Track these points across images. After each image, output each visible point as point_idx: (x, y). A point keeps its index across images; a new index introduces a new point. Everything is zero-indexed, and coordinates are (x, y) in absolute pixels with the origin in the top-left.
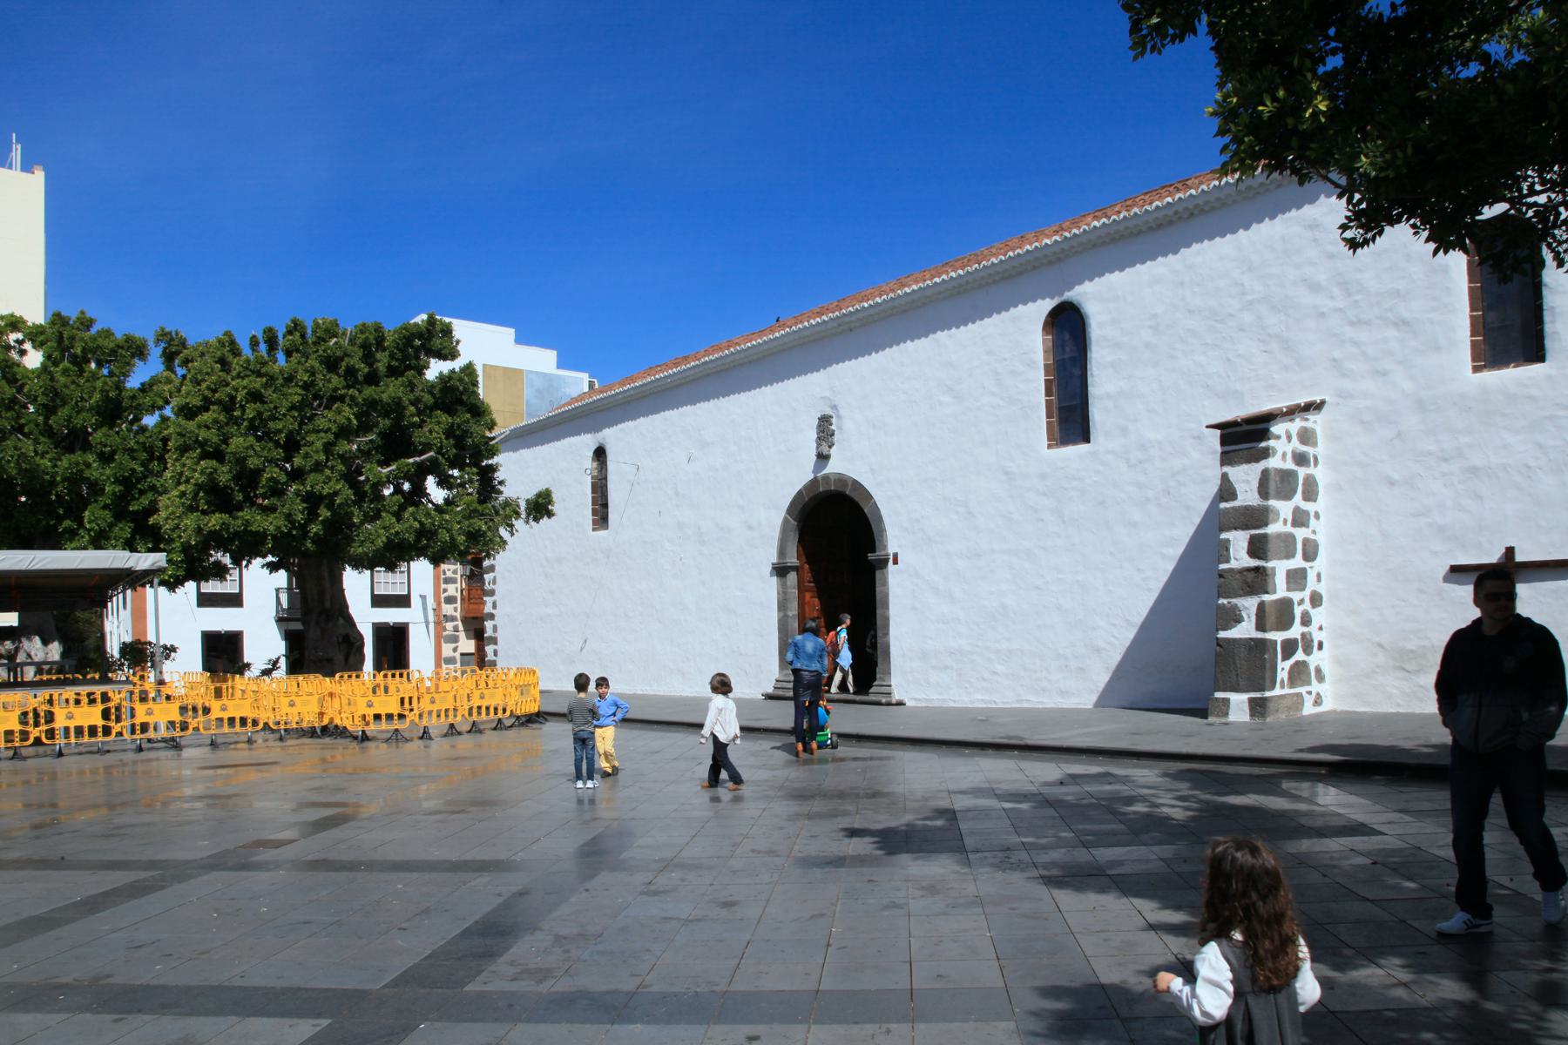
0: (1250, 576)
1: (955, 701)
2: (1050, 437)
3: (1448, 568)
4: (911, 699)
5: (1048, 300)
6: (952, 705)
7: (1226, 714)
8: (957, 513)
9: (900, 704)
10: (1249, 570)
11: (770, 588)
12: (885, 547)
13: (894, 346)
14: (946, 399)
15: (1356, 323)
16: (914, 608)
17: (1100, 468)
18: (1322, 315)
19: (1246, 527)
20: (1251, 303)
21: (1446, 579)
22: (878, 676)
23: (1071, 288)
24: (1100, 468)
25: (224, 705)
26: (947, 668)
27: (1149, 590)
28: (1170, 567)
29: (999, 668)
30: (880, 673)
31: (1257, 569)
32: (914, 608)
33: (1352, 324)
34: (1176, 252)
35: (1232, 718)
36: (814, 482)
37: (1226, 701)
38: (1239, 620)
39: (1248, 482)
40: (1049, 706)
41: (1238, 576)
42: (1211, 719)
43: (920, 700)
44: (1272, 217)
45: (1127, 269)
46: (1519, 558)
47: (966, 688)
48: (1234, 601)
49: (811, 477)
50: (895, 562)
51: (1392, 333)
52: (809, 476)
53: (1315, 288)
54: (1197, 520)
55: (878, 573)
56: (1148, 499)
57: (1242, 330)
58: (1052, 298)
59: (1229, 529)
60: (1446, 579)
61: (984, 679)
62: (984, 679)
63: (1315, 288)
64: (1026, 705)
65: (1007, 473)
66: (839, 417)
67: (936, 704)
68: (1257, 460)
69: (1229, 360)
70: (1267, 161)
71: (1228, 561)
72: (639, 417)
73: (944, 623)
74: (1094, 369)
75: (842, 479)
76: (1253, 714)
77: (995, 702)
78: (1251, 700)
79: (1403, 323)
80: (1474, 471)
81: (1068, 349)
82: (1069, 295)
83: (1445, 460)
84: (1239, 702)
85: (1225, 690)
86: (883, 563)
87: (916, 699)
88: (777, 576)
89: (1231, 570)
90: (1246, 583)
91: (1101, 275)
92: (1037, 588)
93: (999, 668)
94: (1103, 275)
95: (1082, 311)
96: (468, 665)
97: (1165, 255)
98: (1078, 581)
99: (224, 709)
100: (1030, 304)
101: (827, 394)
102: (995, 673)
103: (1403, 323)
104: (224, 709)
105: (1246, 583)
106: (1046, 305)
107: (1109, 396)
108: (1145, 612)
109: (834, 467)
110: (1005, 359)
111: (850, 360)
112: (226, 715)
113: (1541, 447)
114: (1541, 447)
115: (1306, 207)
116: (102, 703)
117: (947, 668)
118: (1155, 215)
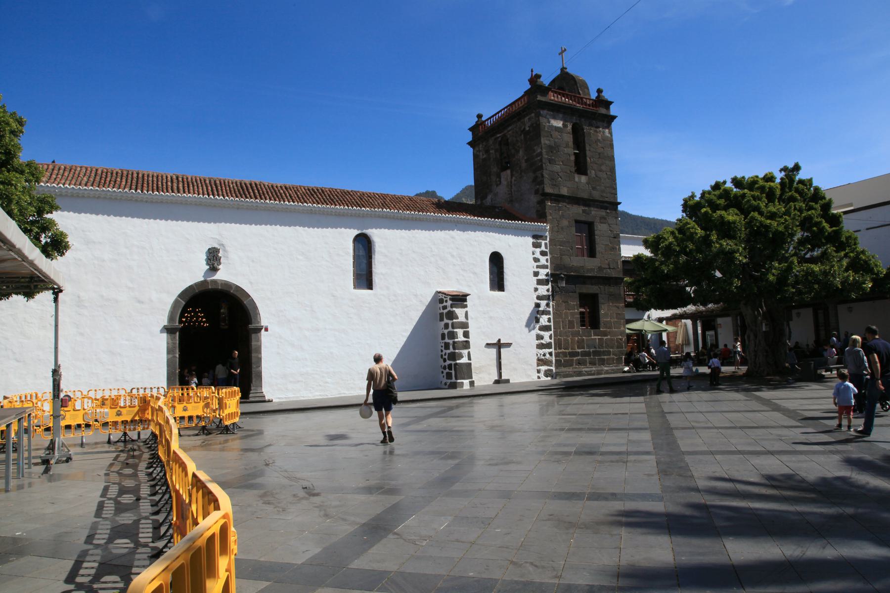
0: (465, 343)
1: (304, 397)
2: (354, 285)
3: (485, 344)
4: (277, 398)
5: (356, 230)
6: (303, 399)
7: (463, 387)
8: (306, 310)
9: (269, 401)
10: (464, 341)
11: (162, 342)
12: (259, 322)
13: (212, 223)
14: (300, 257)
15: (464, 270)
16: (278, 353)
17: (377, 300)
18: (454, 265)
19: (462, 328)
20: (434, 255)
21: (485, 347)
22: (252, 388)
23: (367, 229)
24: (377, 300)
25: (185, 406)
26: (298, 382)
27: (397, 348)
28: (405, 339)
29: (329, 380)
30: (253, 386)
31: (466, 341)
32: (278, 353)
33: (462, 270)
34: (409, 230)
35: (464, 388)
36: (204, 282)
37: (462, 383)
38: (463, 357)
39: (462, 314)
40: (355, 395)
41: (461, 343)
42: (458, 389)
43: (282, 398)
44: (441, 231)
45: (248, 225)
46: (502, 342)
47: (310, 390)
48: (460, 351)
49: (202, 279)
50: (266, 330)
51: (472, 275)
52: (200, 278)
53: (453, 256)
54: (415, 324)
55: (253, 336)
56: (397, 314)
57: (431, 263)
58: (358, 230)
59: (457, 328)
60: (485, 347)
61: (320, 386)
62: (320, 386)
63: (453, 256)
64: (343, 395)
65: (334, 296)
66: (225, 251)
67: (295, 399)
68: (464, 308)
69: (426, 271)
70: (810, 235)
71: (458, 338)
72: (446, 230)
73: (297, 360)
74: (376, 262)
75: (227, 284)
76: (470, 386)
77: (327, 395)
78: (470, 381)
79: (475, 273)
80: (491, 318)
81: (361, 251)
82: (365, 231)
83: (484, 313)
84: (466, 382)
85: (461, 379)
86: (258, 330)
87: (279, 398)
88: (167, 333)
89: (459, 341)
90: (463, 345)
91: (381, 228)
92: (348, 345)
93: (329, 380)
94: (211, 223)
95: (371, 239)
96: (555, 350)
97: (405, 229)
98: (368, 344)
99: (185, 409)
100: (348, 229)
101: (217, 237)
102: (327, 382)
103: (475, 273)
104: (185, 409)
105: (463, 345)
106: (356, 232)
107: (382, 274)
108: (395, 356)
109: (222, 275)
110: (335, 248)
111: (502, 234)
112: (186, 414)
113: (504, 313)
114: (504, 313)
115: (451, 231)
116: (156, 396)
117: (298, 382)
118: (172, 198)
